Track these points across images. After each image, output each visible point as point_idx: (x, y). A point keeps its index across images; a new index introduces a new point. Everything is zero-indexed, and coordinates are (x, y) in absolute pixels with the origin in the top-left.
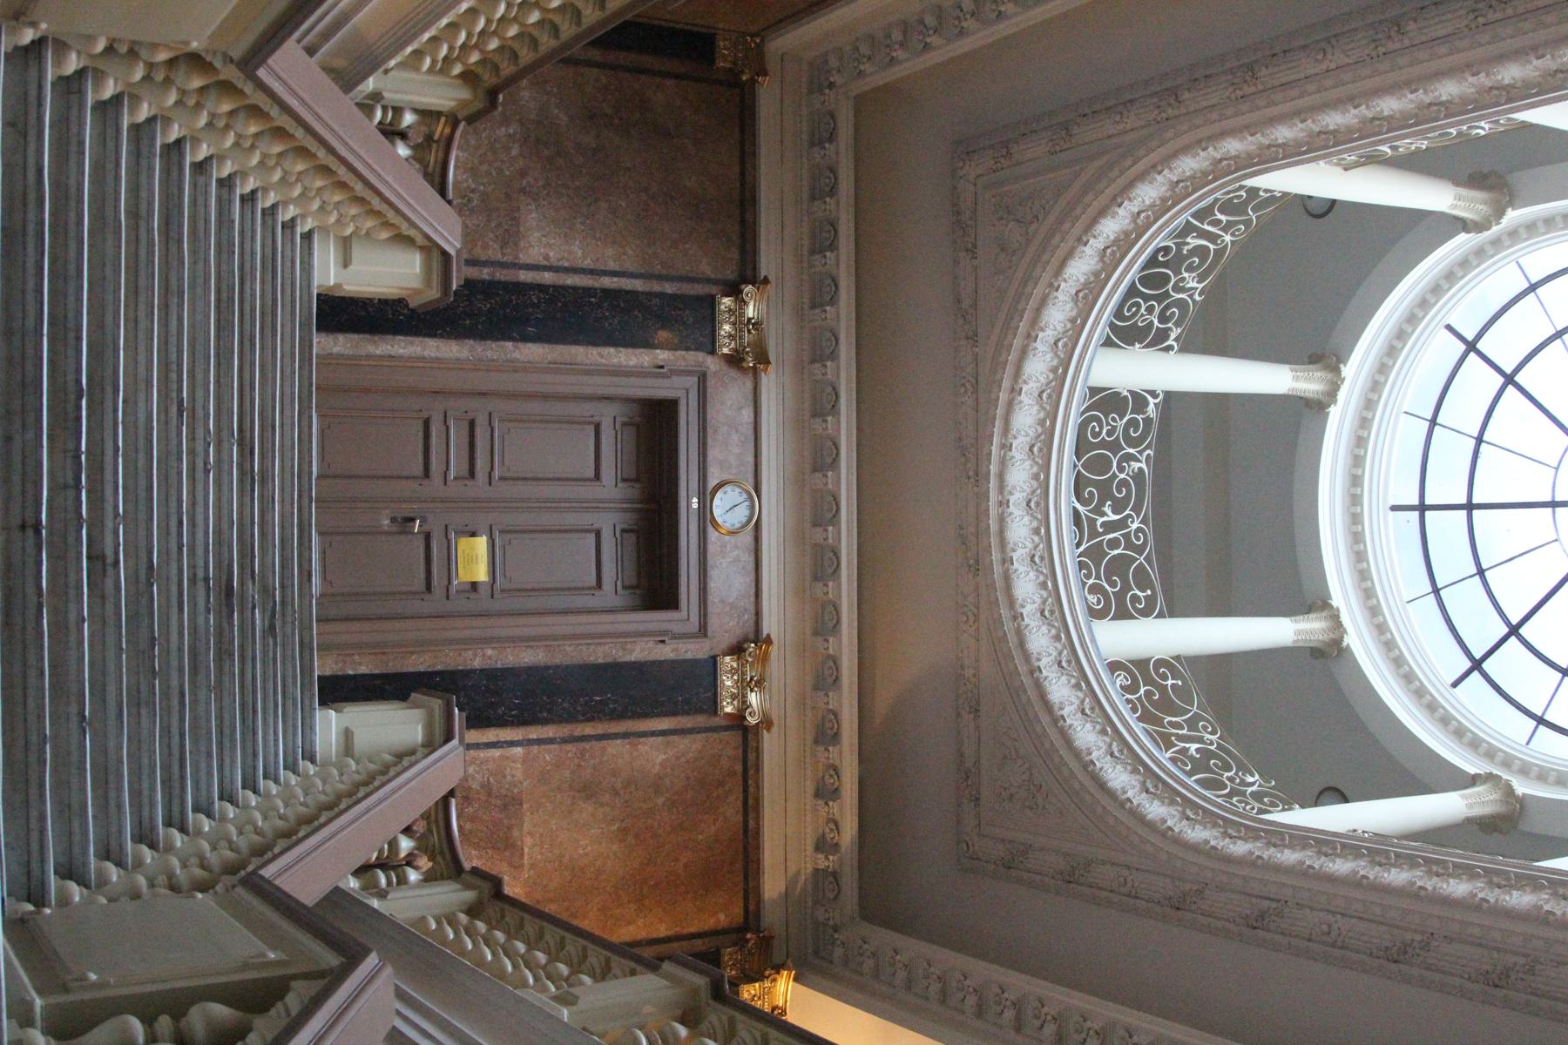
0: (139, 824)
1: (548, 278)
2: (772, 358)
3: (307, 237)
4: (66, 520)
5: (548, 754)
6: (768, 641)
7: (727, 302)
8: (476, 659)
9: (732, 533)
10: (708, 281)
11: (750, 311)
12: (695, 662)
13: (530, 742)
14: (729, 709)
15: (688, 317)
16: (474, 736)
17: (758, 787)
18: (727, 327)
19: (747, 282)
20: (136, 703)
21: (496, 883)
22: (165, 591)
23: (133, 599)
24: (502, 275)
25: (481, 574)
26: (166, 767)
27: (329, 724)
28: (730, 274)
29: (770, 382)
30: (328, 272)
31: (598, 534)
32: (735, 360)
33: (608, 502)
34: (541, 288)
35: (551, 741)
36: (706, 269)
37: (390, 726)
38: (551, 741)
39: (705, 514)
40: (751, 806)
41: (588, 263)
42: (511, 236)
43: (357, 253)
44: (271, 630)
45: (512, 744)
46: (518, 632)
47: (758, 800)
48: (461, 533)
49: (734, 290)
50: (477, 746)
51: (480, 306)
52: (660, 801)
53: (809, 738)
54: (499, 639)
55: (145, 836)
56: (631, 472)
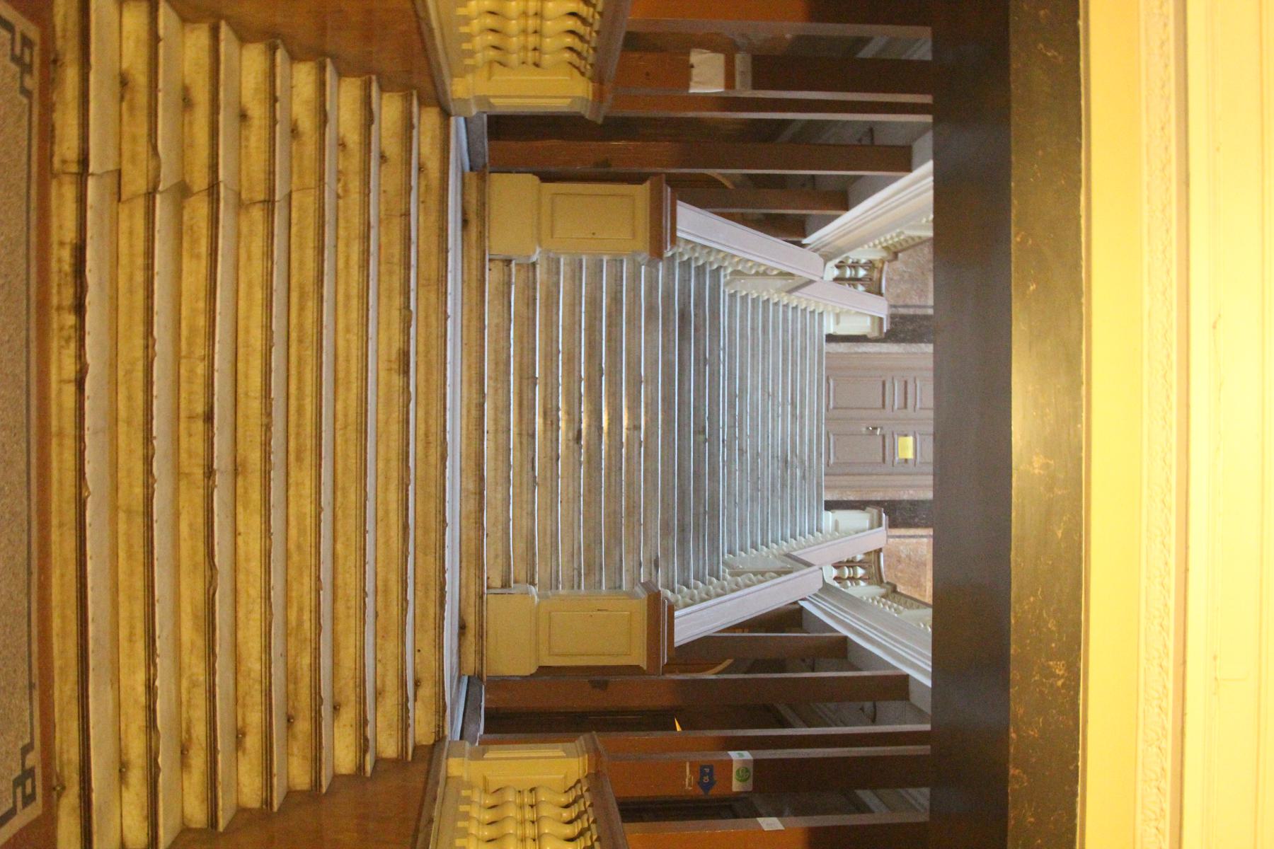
0: (752, 543)
4: (732, 437)
8: (906, 495)
20: (752, 501)
22: (763, 461)
23: (752, 463)
25: (910, 455)
26: (762, 524)
27: (829, 518)
30: (830, 327)
43: (842, 318)
44: (803, 477)
45: (922, 536)
48: (899, 435)
55: (754, 546)
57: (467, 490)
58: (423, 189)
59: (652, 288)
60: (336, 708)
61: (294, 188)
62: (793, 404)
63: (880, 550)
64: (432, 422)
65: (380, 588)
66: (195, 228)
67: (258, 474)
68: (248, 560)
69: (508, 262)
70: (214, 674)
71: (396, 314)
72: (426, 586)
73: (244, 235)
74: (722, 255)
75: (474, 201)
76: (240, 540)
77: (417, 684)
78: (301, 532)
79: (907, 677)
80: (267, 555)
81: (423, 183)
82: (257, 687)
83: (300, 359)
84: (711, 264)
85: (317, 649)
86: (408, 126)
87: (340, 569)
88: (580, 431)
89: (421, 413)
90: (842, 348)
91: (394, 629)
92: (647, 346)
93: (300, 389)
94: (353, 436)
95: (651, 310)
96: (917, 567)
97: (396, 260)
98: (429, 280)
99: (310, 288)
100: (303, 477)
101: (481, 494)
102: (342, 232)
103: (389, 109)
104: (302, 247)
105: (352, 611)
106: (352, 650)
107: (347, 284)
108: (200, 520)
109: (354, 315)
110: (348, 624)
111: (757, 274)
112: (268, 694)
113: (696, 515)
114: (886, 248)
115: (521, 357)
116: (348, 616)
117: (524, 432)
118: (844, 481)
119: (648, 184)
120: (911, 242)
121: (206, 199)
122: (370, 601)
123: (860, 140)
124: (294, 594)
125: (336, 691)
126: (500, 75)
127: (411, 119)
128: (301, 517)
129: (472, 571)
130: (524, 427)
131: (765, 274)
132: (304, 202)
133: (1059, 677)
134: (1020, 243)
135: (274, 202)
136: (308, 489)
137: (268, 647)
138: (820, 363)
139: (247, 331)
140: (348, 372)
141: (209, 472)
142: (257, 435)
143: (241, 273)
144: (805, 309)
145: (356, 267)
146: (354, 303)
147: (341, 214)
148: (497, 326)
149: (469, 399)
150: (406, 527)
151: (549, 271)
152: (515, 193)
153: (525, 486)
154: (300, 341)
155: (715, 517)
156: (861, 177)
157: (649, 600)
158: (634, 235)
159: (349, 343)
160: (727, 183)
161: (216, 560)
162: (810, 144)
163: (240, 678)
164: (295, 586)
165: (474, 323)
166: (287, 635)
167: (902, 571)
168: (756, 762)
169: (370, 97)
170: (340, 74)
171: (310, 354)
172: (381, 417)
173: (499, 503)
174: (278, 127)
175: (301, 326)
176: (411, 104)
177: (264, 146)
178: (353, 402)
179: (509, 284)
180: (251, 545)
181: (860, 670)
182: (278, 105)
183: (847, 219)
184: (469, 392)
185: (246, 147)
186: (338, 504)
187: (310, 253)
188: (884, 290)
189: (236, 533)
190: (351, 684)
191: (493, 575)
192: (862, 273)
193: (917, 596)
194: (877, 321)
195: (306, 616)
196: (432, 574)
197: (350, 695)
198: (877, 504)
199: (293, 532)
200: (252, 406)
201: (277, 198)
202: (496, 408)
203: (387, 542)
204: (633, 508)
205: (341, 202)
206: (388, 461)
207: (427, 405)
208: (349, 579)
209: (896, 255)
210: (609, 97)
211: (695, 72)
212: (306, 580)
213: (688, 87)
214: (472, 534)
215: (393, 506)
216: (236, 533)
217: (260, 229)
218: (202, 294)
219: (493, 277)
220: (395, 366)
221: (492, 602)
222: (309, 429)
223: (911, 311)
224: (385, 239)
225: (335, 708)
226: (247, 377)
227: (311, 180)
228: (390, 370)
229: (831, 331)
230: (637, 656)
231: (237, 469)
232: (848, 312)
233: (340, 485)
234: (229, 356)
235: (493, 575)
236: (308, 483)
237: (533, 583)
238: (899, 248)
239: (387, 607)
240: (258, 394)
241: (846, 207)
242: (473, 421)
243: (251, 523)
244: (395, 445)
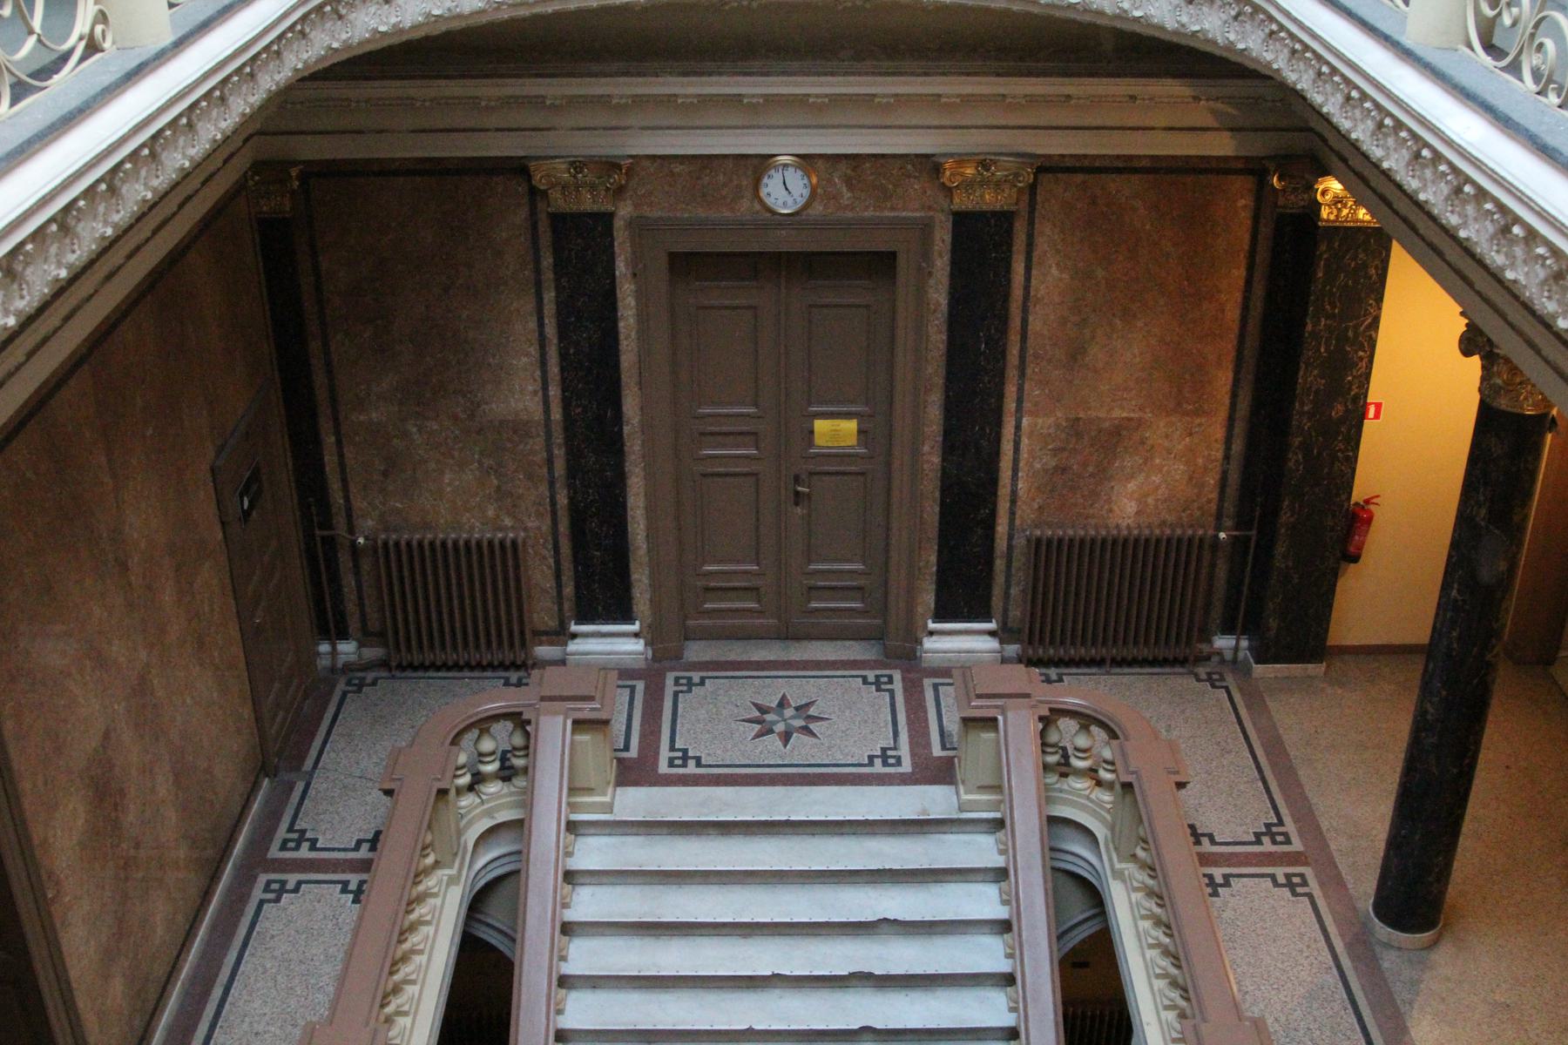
45: (1018, 427)
48: (811, 443)
96: (1079, 435)
156: (30, 76)
167: (1085, 465)
223: (559, 452)
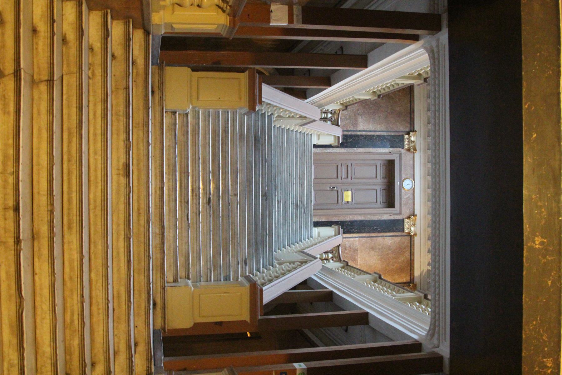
1: (364, 133)
2: (417, 149)
3: (311, 135)
5: (364, 240)
6: (416, 215)
7: (406, 136)
8: (348, 218)
9: (408, 190)
10: (402, 132)
11: (412, 138)
12: (399, 220)
13: (360, 237)
14: (407, 231)
15: (396, 141)
16: (345, 235)
17: (414, 250)
18: (407, 142)
19: (411, 131)
21: (347, 263)
24: (353, 133)
27: (316, 231)
28: (408, 130)
29: (417, 155)
30: (315, 141)
31: (376, 190)
32: (408, 150)
33: (379, 183)
34: (362, 136)
35: (364, 237)
36: (402, 129)
37: (328, 231)
38: (364, 237)
39: (401, 186)
40: (412, 254)
41: (373, 129)
42: (355, 124)
43: (321, 137)
45: (356, 237)
46: (354, 213)
47: (414, 253)
48: (345, 190)
49: (408, 134)
50: (345, 238)
51: (349, 141)
52: (390, 252)
53: (427, 239)
54: (353, 214)
55: (284, 247)
56: (384, 176)
57: (156, 233)
58: (134, 74)
59: (242, 125)
60: (93, 365)
61: (64, 73)
62: (300, 179)
63: (340, 245)
64: (142, 202)
65: (115, 295)
66: (6, 96)
67: (46, 239)
68: (41, 289)
69: (174, 113)
70: (23, 359)
71: (121, 144)
72: (140, 292)
73: (36, 100)
74: (275, 108)
75: (157, 81)
76: (37, 278)
77: (136, 345)
78: (72, 269)
79: (367, 313)
80: (53, 286)
81: (135, 71)
82: (49, 361)
83: (69, 172)
84: (268, 112)
85: (82, 336)
86: (128, 39)
87: (94, 287)
88: (209, 199)
89: (135, 197)
90: (319, 150)
91: (124, 317)
92: (240, 153)
93: (69, 188)
94: (99, 212)
95: (241, 135)
96: (354, 251)
97: (121, 113)
98: (139, 124)
99: (74, 130)
100: (72, 238)
101: (163, 234)
102: (91, 98)
103: (117, 29)
104: (69, 107)
105: (101, 311)
106: (101, 332)
107: (95, 128)
108: (12, 269)
109: (99, 145)
110: (99, 317)
111: (289, 117)
112: (55, 365)
113: (263, 236)
114: (342, 104)
115: (181, 162)
116: (99, 314)
117: (183, 201)
118: (320, 212)
119: (247, 73)
120: (355, 101)
121: (13, 79)
122: (110, 305)
123: (336, 52)
124: (68, 305)
125: (93, 355)
126: (179, 12)
127: (129, 35)
128: (71, 261)
129: (159, 275)
130: (183, 198)
131: (293, 117)
132: (71, 81)
133: (548, 368)
134: (527, 109)
135: (53, 80)
136: (75, 245)
137: (54, 339)
138: (311, 158)
139: (38, 156)
140: (96, 177)
141: (18, 241)
142: (45, 216)
143: (34, 122)
144: (304, 133)
145: (100, 119)
146: (99, 138)
147: (91, 88)
148: (169, 146)
149: (156, 185)
150: (129, 261)
151: (194, 118)
152: (178, 77)
153: (183, 229)
154: (69, 161)
155: (271, 235)
157: (251, 286)
158: (240, 99)
159: (96, 161)
160: (264, 72)
161: (23, 293)
162: (310, 53)
163: (39, 357)
164: (69, 300)
165: (158, 145)
166: (65, 328)
167: (347, 254)
168: (309, 370)
169: (107, 21)
170: (90, 9)
171: (75, 168)
172: (114, 201)
173: (171, 238)
174: (55, 37)
175: (69, 152)
176: (129, 27)
177: (47, 49)
178: (99, 194)
179: (175, 124)
180: (43, 280)
181: (344, 310)
182: (55, 24)
183: (329, 90)
184: (156, 181)
185: (37, 49)
186: (92, 251)
187: (74, 110)
188: (340, 124)
189: (34, 274)
190: (101, 351)
191: (169, 276)
192: (329, 115)
193: (354, 266)
194: (337, 138)
195: (76, 317)
196: (143, 284)
197: (101, 357)
198: (336, 223)
199: (67, 270)
200: (42, 200)
201: (55, 78)
202: (169, 190)
203: (119, 270)
204: (234, 235)
205: (91, 81)
206: (118, 225)
207: (139, 192)
208: (99, 294)
209: (346, 107)
210: (238, 25)
211: (272, 14)
212: (75, 297)
213: (270, 22)
214: (158, 255)
215: (122, 250)
216: (34, 274)
217: (45, 96)
218: (11, 136)
219: (167, 120)
220: (122, 172)
221: (169, 290)
222: (75, 211)
223: (350, 133)
224: (116, 102)
225: (92, 365)
226: (38, 182)
227: (74, 69)
228: (119, 174)
229: (316, 143)
230: (246, 316)
231: (34, 237)
232: (324, 134)
233: (92, 240)
234: (28, 171)
235: (169, 276)
236: (75, 241)
237: (189, 279)
238: (348, 104)
239: (119, 306)
240: (46, 193)
241: (330, 85)
242: (158, 197)
243: (43, 267)
244: (122, 216)
